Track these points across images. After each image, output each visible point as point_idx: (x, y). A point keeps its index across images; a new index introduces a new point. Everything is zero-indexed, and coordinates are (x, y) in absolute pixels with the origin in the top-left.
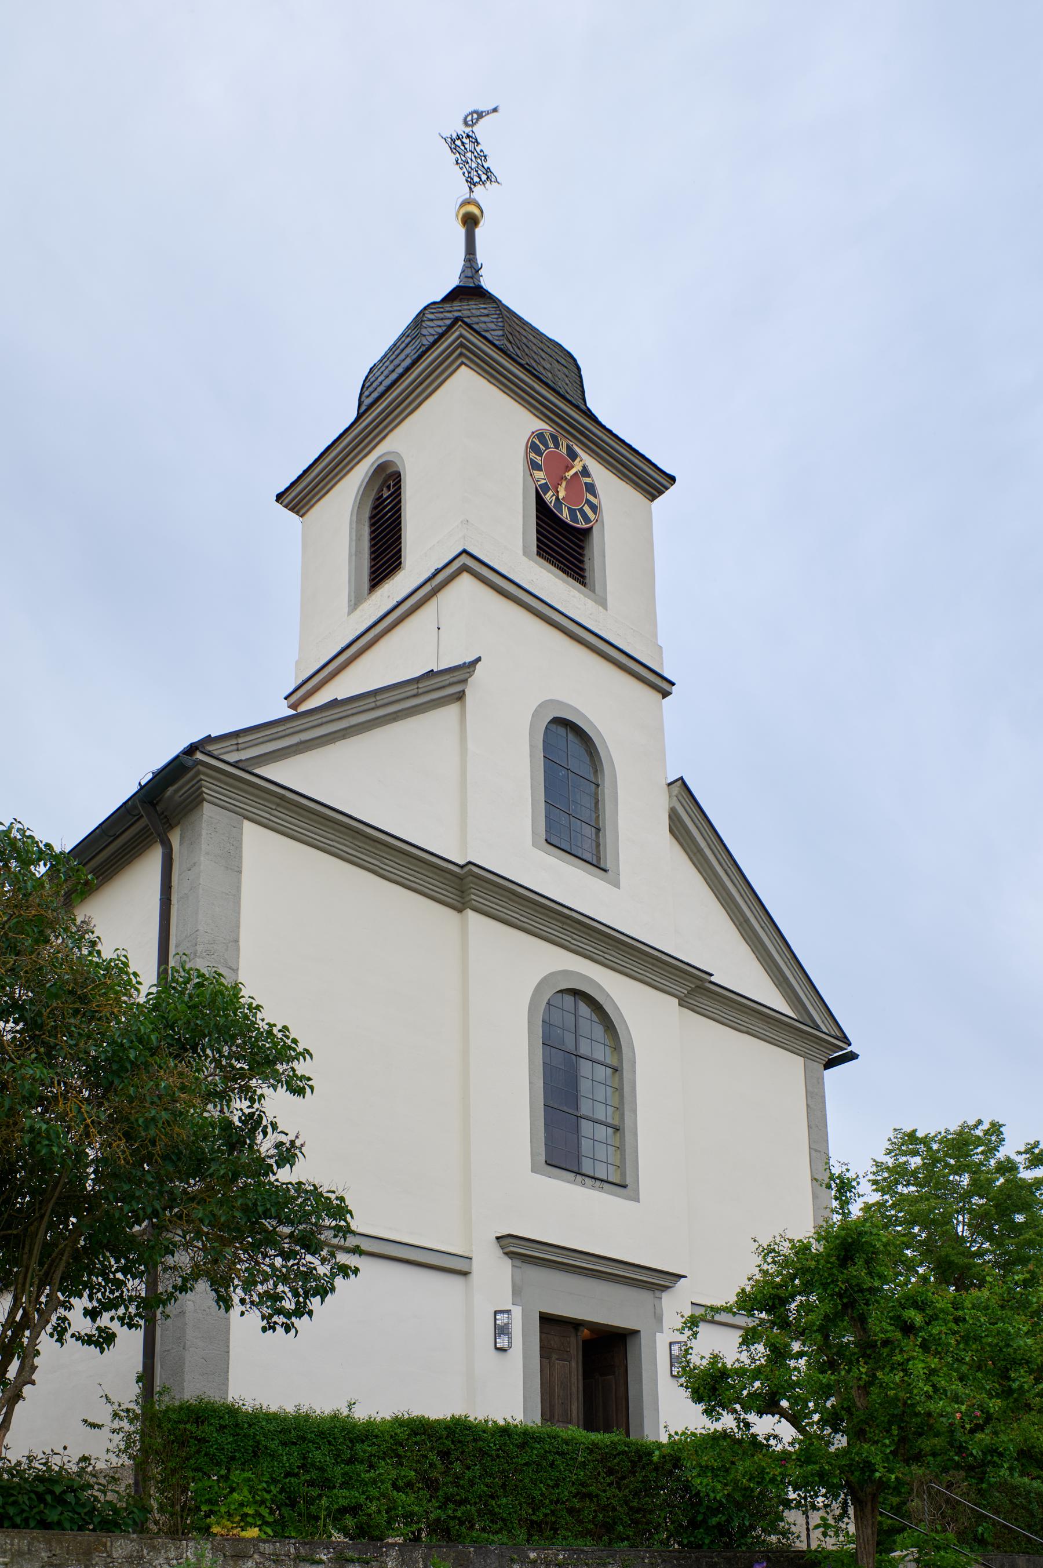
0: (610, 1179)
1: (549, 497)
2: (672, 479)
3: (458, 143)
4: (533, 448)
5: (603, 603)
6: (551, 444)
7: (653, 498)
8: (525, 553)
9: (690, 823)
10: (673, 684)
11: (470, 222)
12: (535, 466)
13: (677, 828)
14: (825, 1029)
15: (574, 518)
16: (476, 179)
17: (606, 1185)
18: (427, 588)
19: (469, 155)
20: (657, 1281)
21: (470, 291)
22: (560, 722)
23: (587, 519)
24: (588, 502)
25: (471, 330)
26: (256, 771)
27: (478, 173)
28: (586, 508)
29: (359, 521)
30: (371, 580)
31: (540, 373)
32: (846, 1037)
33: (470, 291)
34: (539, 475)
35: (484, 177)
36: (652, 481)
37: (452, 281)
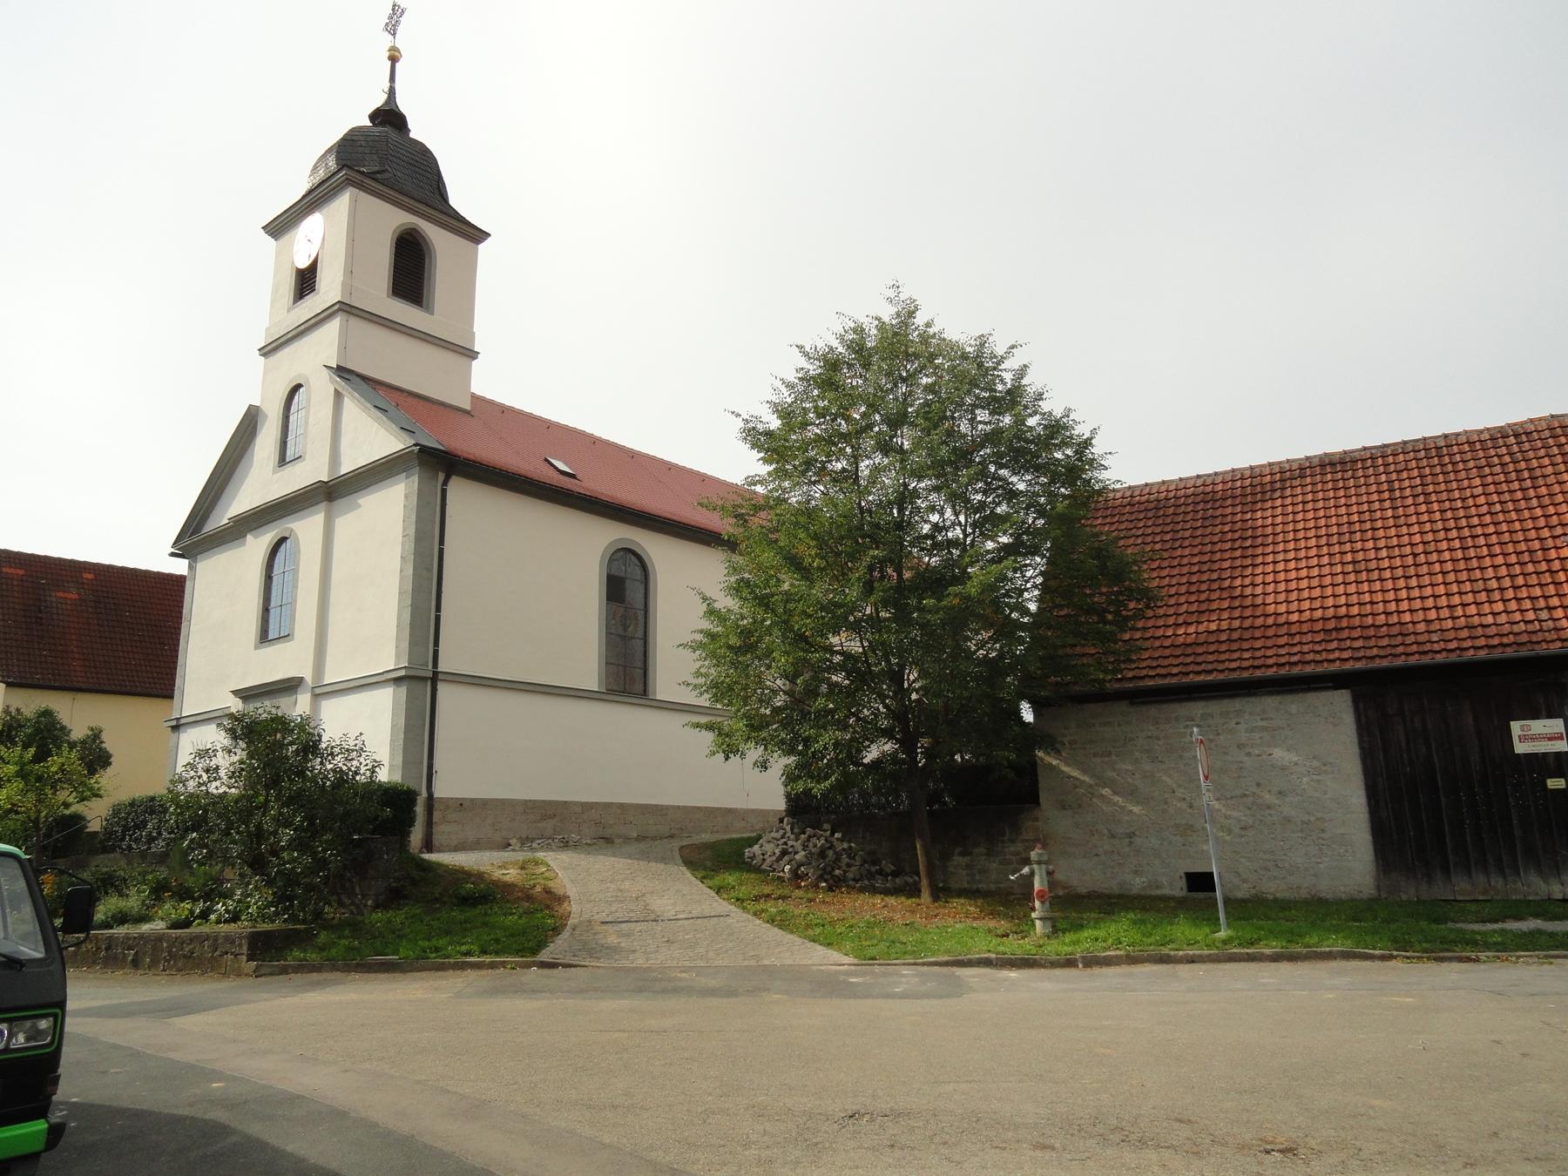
11: (394, 60)
21: (389, 117)
33: (389, 117)
36: (476, 235)
37: (379, 100)
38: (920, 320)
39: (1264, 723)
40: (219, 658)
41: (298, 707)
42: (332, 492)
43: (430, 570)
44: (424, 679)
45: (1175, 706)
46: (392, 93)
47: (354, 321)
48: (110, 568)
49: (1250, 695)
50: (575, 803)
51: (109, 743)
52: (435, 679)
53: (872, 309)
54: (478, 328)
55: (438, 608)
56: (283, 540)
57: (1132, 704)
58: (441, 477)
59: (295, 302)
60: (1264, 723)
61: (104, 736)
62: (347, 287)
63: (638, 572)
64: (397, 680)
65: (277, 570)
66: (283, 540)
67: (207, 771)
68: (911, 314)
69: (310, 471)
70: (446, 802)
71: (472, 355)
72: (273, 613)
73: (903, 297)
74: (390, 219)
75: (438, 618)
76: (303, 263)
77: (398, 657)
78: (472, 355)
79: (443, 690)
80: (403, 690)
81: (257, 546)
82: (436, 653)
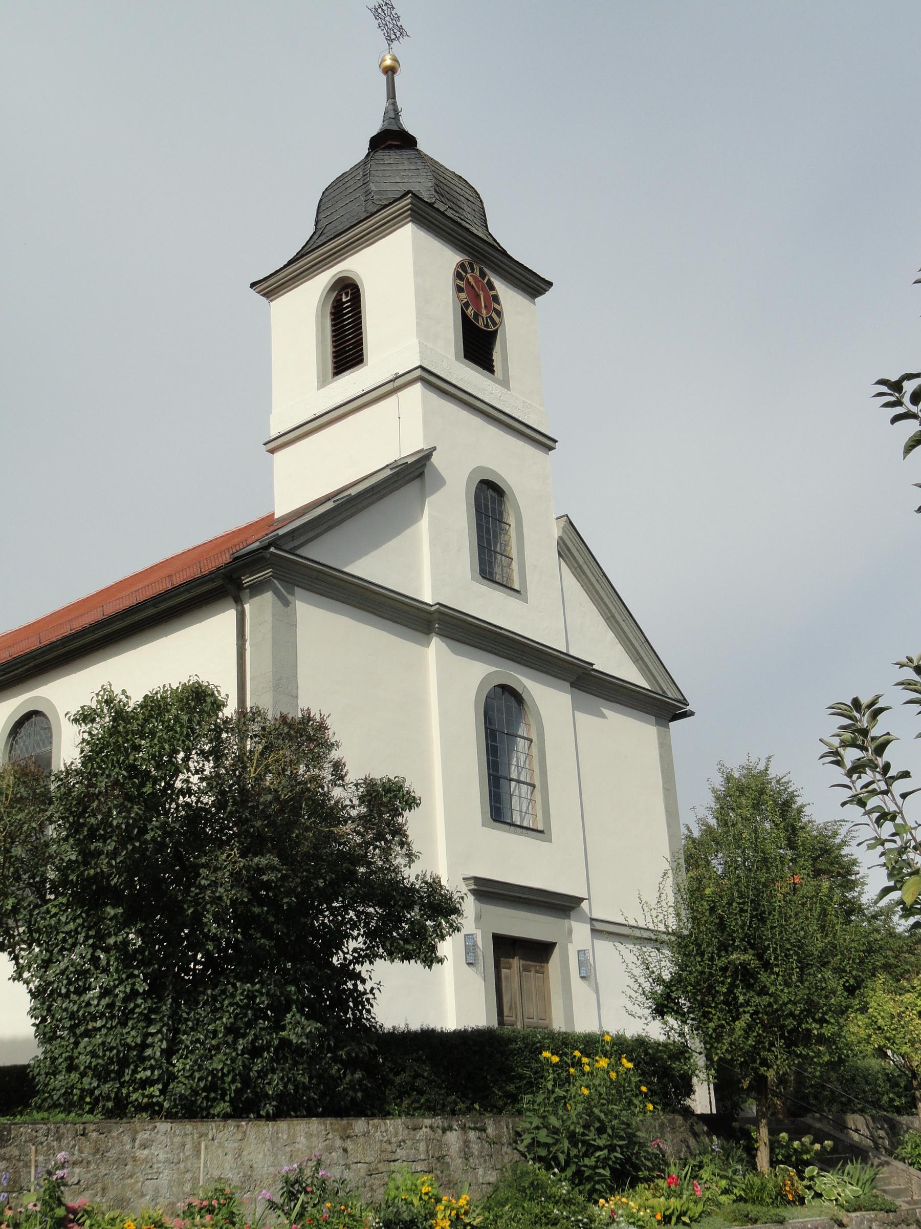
0: (525, 824)
1: (470, 312)
2: (550, 284)
3: (380, 10)
4: (458, 276)
5: (505, 383)
6: (469, 271)
7: (536, 297)
8: (457, 359)
9: (574, 550)
10: (555, 441)
11: (390, 71)
12: (459, 289)
13: (564, 551)
14: (670, 696)
15: (487, 326)
16: (393, 37)
17: (530, 832)
18: (390, 387)
19: (387, 18)
20: (562, 905)
21: (393, 140)
22: (483, 482)
23: (495, 324)
24: (495, 309)
25: (398, 181)
26: (345, 570)
27: (394, 32)
28: (494, 315)
29: (323, 316)
30: (335, 368)
31: (449, 214)
32: (685, 699)
33: (393, 140)
34: (463, 295)
35: (398, 34)
46: (393, 112)
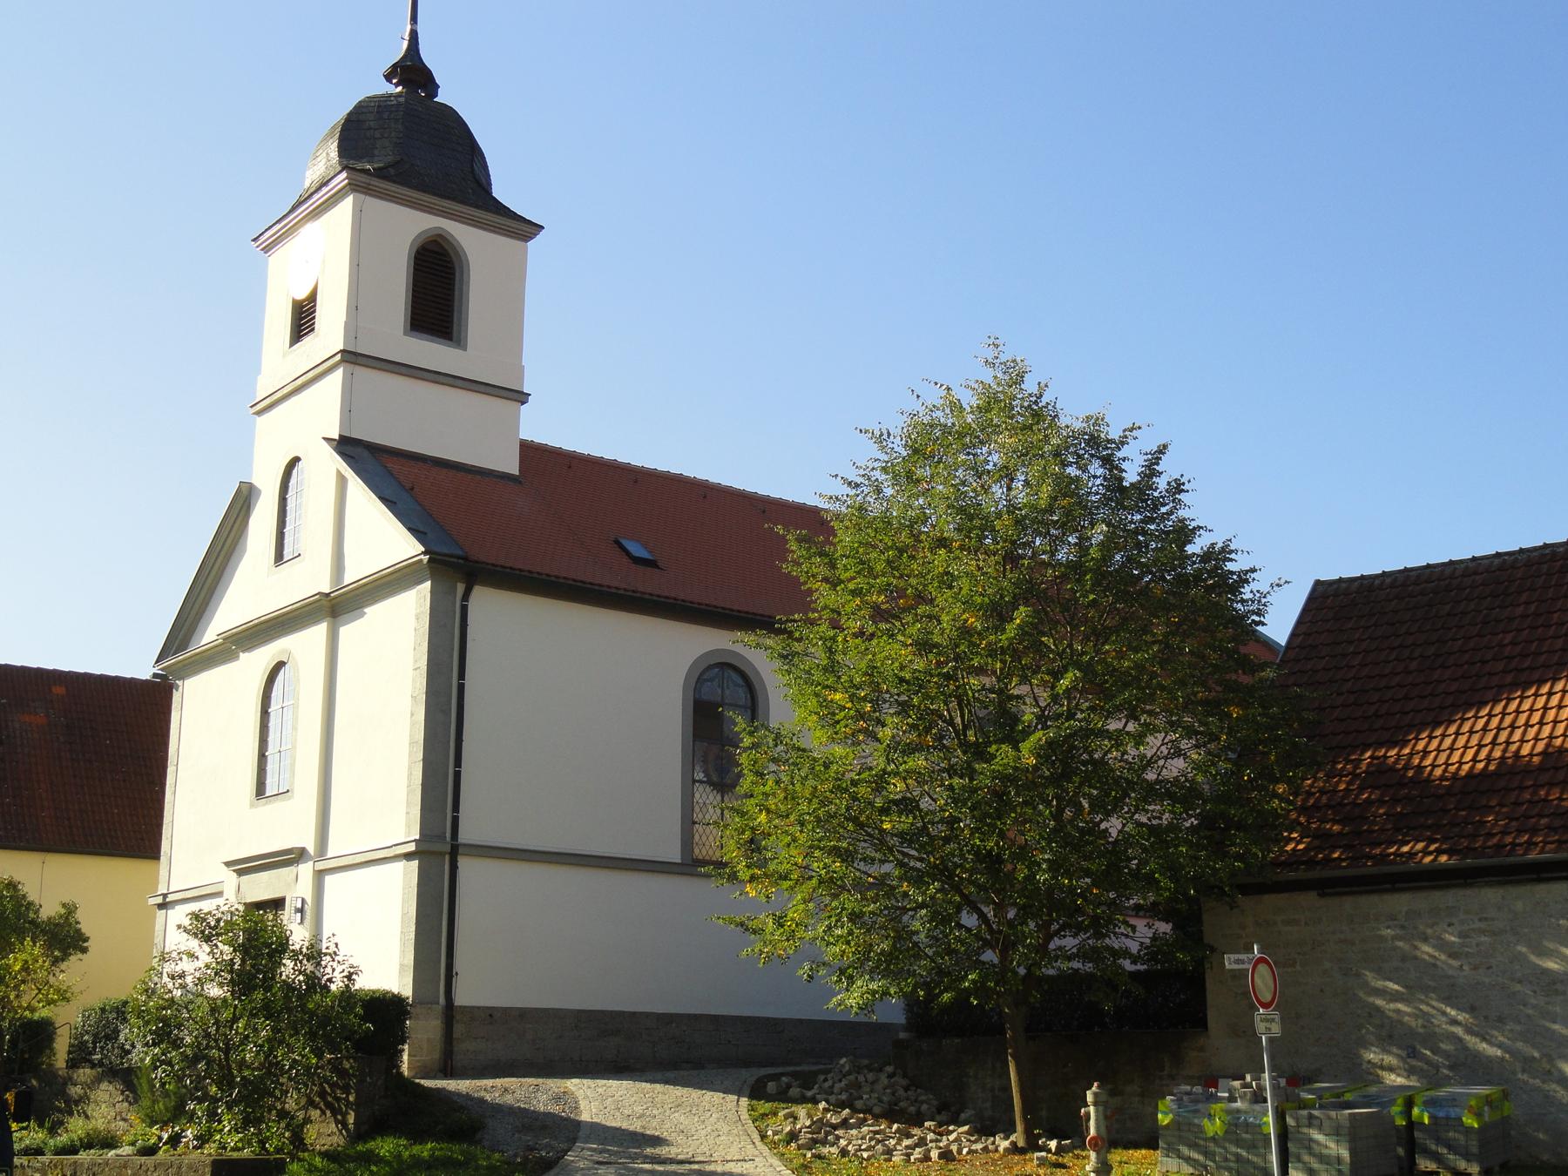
21: (412, 72)
33: (412, 72)
36: (525, 229)
38: (1030, 386)
39: (1483, 925)
40: (211, 821)
41: (295, 884)
42: (337, 606)
43: (447, 713)
44: (442, 854)
45: (1375, 898)
46: (414, 36)
47: (363, 373)
48: (87, 677)
49: (1466, 885)
50: (647, 1015)
51: (86, 923)
52: (455, 851)
53: (964, 377)
54: (529, 359)
55: (458, 763)
56: (280, 665)
57: (1322, 895)
58: (461, 588)
59: (291, 345)
60: (1483, 925)
61: (79, 915)
62: (352, 328)
63: (742, 695)
64: (408, 856)
65: (274, 708)
66: (280, 665)
67: (173, 978)
68: (1019, 379)
69: (308, 578)
70: (471, 1011)
71: (521, 397)
72: (271, 767)
73: (1003, 358)
74: (409, 224)
75: (457, 775)
76: (302, 294)
77: (408, 826)
78: (521, 397)
79: (464, 863)
80: (416, 863)
81: (256, 662)
82: (455, 821)
